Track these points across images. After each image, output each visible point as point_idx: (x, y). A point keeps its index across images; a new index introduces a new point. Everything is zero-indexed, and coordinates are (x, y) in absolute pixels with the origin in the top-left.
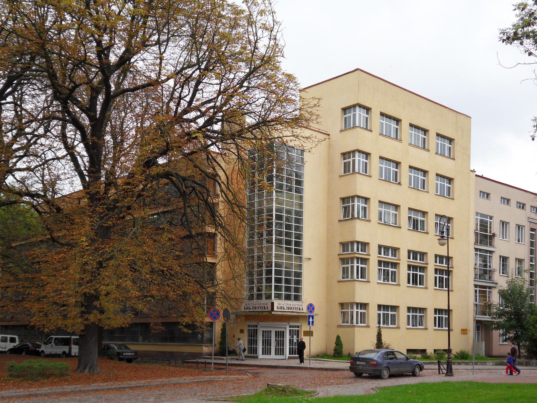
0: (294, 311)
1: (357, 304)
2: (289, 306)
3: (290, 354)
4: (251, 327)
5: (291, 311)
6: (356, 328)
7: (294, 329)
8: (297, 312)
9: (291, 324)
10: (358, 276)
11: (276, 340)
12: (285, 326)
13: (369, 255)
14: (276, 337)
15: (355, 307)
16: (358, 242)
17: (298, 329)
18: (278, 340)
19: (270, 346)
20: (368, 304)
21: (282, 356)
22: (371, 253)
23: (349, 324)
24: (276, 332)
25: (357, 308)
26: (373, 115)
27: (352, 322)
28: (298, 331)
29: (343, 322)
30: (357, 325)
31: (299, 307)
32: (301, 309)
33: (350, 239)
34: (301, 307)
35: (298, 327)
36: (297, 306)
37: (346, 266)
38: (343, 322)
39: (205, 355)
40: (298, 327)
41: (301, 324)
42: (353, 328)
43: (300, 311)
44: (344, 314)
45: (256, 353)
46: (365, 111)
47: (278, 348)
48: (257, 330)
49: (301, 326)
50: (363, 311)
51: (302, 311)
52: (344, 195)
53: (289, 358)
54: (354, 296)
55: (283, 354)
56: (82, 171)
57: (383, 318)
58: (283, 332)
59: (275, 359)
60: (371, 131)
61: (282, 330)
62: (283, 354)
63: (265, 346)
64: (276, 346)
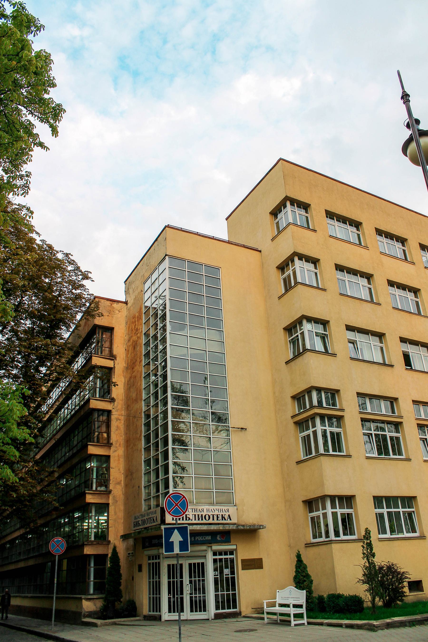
0: (211, 521)
1: (333, 498)
2: (200, 514)
3: (217, 608)
4: (220, 554)
5: (204, 521)
6: (334, 546)
7: (229, 557)
8: (219, 524)
9: (216, 547)
10: (328, 447)
11: (191, 582)
12: (203, 554)
13: (343, 410)
14: (190, 577)
15: (328, 504)
16: (319, 390)
17: (232, 556)
18: (195, 581)
19: (182, 593)
20: (354, 496)
21: (203, 613)
22: (344, 407)
23: (323, 539)
24: (190, 565)
25: (333, 506)
26: (314, 213)
27: (327, 535)
28: (232, 561)
29: (315, 537)
30: (337, 539)
31: (221, 513)
32: (226, 517)
33: (304, 387)
34: (227, 514)
35: (231, 553)
36: (216, 513)
37: (305, 433)
38: (315, 537)
39: (85, 616)
40: (231, 553)
41: (234, 547)
42: (329, 545)
43: (224, 522)
44: (315, 522)
45: (160, 611)
46: (377, 339)
47: (156, 594)
48: (159, 563)
49: (236, 550)
50: (346, 511)
51: (229, 521)
52: (287, 322)
53: (217, 616)
54: (322, 485)
55: (205, 611)
56: (63, 399)
57: (390, 520)
58: (203, 564)
59: (190, 620)
60: (315, 231)
61: (200, 561)
62: (205, 611)
63: (174, 596)
64: (191, 594)
